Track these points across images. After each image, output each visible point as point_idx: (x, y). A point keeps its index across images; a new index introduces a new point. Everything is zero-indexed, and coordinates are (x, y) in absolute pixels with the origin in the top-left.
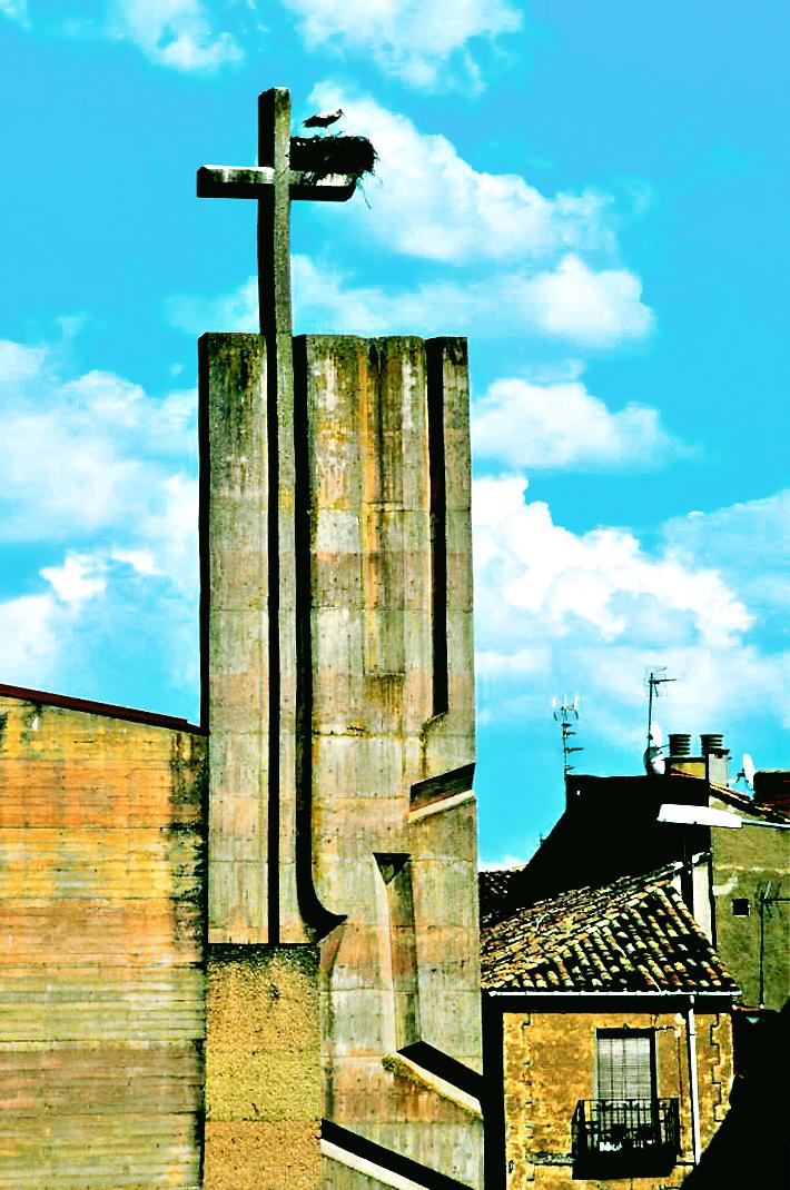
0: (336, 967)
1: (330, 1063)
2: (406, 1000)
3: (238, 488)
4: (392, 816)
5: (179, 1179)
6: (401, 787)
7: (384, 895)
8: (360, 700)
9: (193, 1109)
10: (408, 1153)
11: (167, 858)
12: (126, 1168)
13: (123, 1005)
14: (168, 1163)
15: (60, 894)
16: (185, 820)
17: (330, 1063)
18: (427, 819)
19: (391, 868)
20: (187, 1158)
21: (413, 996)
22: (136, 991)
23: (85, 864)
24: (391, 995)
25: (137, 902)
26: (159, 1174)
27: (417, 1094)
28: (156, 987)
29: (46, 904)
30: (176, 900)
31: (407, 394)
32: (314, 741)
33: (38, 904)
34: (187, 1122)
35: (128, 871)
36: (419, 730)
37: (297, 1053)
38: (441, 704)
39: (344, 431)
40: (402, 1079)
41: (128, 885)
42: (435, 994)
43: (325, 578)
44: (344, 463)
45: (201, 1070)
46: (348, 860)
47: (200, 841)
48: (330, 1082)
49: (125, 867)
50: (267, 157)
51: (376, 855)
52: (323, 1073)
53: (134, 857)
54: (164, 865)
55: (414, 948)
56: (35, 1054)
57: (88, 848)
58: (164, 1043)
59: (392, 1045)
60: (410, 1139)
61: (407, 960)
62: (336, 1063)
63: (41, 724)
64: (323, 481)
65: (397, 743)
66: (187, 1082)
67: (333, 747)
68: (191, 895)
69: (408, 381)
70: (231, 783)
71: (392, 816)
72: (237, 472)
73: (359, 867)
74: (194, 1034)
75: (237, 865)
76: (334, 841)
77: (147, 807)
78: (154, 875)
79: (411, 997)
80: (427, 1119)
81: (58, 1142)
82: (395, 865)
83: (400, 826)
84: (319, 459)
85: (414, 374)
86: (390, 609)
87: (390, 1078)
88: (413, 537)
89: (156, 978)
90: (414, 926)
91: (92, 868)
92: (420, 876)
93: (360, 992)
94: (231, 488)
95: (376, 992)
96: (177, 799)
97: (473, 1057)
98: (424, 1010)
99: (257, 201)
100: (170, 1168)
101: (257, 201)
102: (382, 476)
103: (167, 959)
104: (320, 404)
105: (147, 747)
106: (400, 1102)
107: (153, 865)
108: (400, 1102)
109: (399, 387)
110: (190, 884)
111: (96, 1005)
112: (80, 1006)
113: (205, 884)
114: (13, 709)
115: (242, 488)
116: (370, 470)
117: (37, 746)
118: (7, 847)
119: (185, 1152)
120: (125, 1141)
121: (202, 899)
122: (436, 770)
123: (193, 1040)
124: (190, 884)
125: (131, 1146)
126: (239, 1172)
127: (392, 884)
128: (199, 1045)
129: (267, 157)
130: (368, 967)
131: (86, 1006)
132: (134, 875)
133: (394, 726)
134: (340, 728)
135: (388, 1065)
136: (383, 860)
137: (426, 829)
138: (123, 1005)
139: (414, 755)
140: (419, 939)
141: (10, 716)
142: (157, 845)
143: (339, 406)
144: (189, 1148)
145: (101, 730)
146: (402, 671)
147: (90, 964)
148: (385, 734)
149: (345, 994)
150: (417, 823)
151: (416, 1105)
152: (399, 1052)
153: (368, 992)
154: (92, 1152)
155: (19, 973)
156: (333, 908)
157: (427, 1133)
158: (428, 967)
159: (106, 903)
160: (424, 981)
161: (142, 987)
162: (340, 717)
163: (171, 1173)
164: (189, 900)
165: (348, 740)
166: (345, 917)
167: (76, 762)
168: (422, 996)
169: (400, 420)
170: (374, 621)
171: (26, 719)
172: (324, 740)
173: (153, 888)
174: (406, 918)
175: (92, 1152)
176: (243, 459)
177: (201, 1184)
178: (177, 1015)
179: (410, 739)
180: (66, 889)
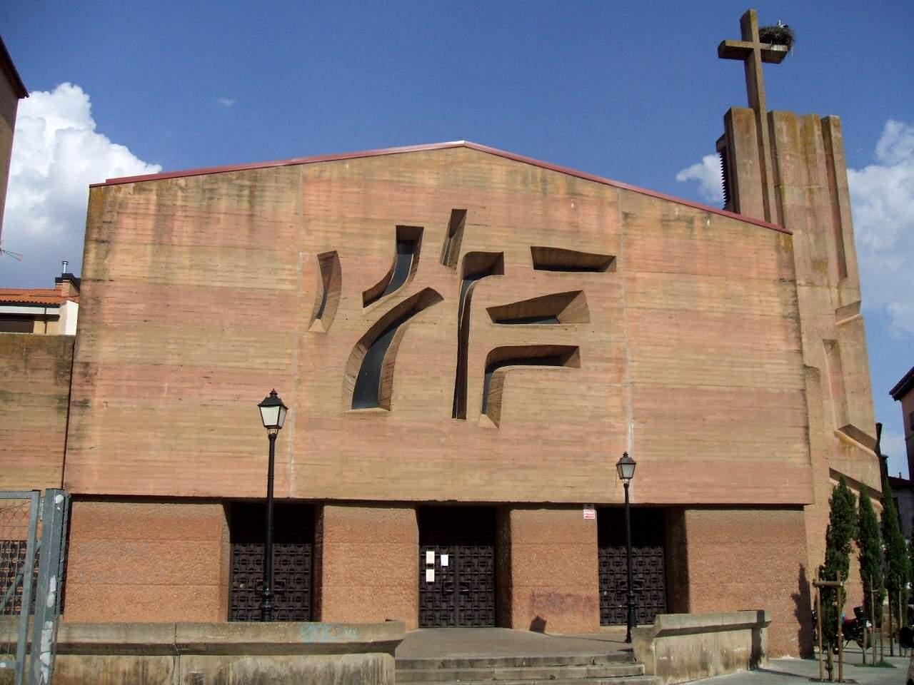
2: (840, 406)
3: (749, 174)
5: (801, 460)
6: (831, 310)
9: (802, 425)
12: (773, 453)
14: (793, 452)
15: (728, 311)
18: (843, 325)
19: (829, 347)
20: (802, 450)
21: (844, 403)
23: (739, 296)
24: (833, 404)
26: (790, 458)
27: (849, 448)
29: (722, 315)
30: (785, 317)
33: (718, 315)
34: (801, 431)
36: (836, 285)
38: (843, 272)
39: (792, 152)
40: (843, 441)
44: (793, 166)
45: (806, 405)
46: (812, 342)
47: (794, 288)
50: (746, 35)
51: (823, 340)
54: (777, 299)
56: (724, 393)
57: (740, 288)
58: (786, 391)
60: (848, 468)
63: (710, 223)
64: (785, 173)
65: (828, 291)
68: (791, 316)
71: (828, 323)
72: (748, 167)
74: (801, 386)
77: (766, 269)
78: (772, 304)
79: (843, 404)
80: (855, 458)
82: (832, 345)
83: (832, 327)
85: (819, 130)
86: (819, 234)
88: (824, 200)
90: (842, 373)
91: (743, 298)
92: (843, 350)
94: (747, 174)
96: (780, 266)
97: (872, 432)
99: (743, 61)
100: (795, 455)
101: (743, 61)
102: (809, 173)
103: (784, 348)
104: (781, 140)
105: (764, 239)
106: (843, 451)
107: (772, 299)
108: (843, 451)
109: (813, 135)
111: (750, 369)
112: (743, 369)
113: (798, 310)
114: (698, 215)
116: (804, 172)
118: (701, 285)
119: (800, 446)
121: (797, 318)
122: (845, 303)
123: (334, 671)
124: (791, 309)
128: (803, 390)
129: (746, 35)
131: (746, 369)
132: (764, 304)
133: (826, 283)
134: (802, 282)
135: (836, 435)
136: (826, 342)
137: (843, 329)
139: (835, 296)
140: (845, 378)
141: (696, 218)
142: (772, 289)
143: (788, 142)
145: (741, 228)
146: (827, 258)
147: (746, 348)
148: (822, 286)
150: (840, 326)
151: (849, 452)
152: (839, 429)
154: (757, 445)
155: (711, 350)
158: (850, 391)
159: (751, 317)
160: (849, 398)
164: (791, 317)
165: (806, 288)
169: (815, 149)
170: (812, 238)
171: (704, 220)
173: (773, 311)
175: (757, 445)
177: (811, 464)
180: (732, 308)
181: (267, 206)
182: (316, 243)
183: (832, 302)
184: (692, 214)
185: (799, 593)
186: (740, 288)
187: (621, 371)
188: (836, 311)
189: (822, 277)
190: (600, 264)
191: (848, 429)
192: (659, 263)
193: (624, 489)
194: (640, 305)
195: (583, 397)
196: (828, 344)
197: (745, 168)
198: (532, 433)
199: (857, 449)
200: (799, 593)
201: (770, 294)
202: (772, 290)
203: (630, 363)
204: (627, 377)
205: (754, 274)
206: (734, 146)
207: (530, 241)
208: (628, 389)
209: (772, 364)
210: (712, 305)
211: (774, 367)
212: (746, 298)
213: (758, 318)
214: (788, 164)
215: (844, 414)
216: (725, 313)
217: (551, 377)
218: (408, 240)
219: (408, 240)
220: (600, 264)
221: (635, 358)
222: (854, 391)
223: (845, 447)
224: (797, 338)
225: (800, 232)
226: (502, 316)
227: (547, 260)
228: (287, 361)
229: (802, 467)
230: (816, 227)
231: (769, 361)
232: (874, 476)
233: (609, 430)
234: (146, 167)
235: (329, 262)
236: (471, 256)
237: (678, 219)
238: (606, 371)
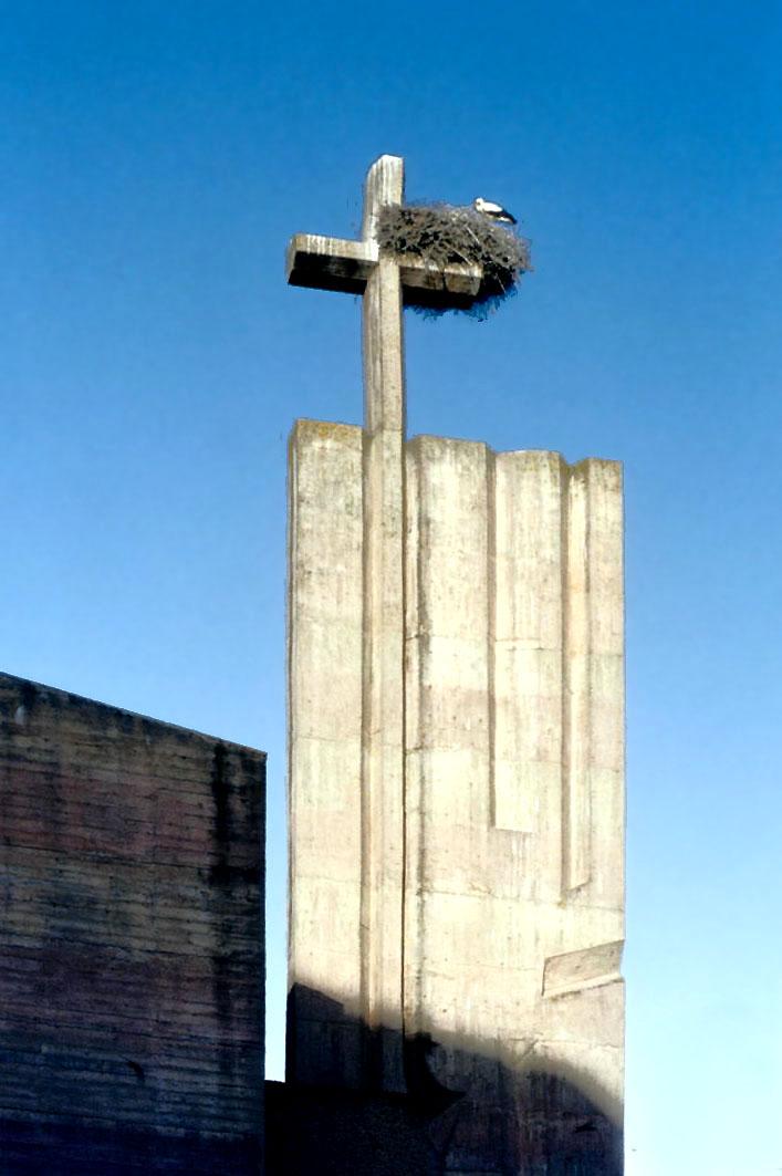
15: (57, 934)
33: (26, 943)
54: (204, 916)
107: (188, 914)
131: (96, 1076)
142: (193, 889)
181: (608, 913)
185: (573, 478)
186: (96, 882)
200: (573, 478)
201: (182, 901)
202: (191, 893)
205: (140, 848)
206: (369, 824)
209: (170, 1068)
210: (11, 916)
211: (175, 1076)
212: (110, 907)
213: (139, 957)
216: (44, 938)
224: (427, 880)
231: (165, 1061)
232: (395, 572)
234: (428, 891)
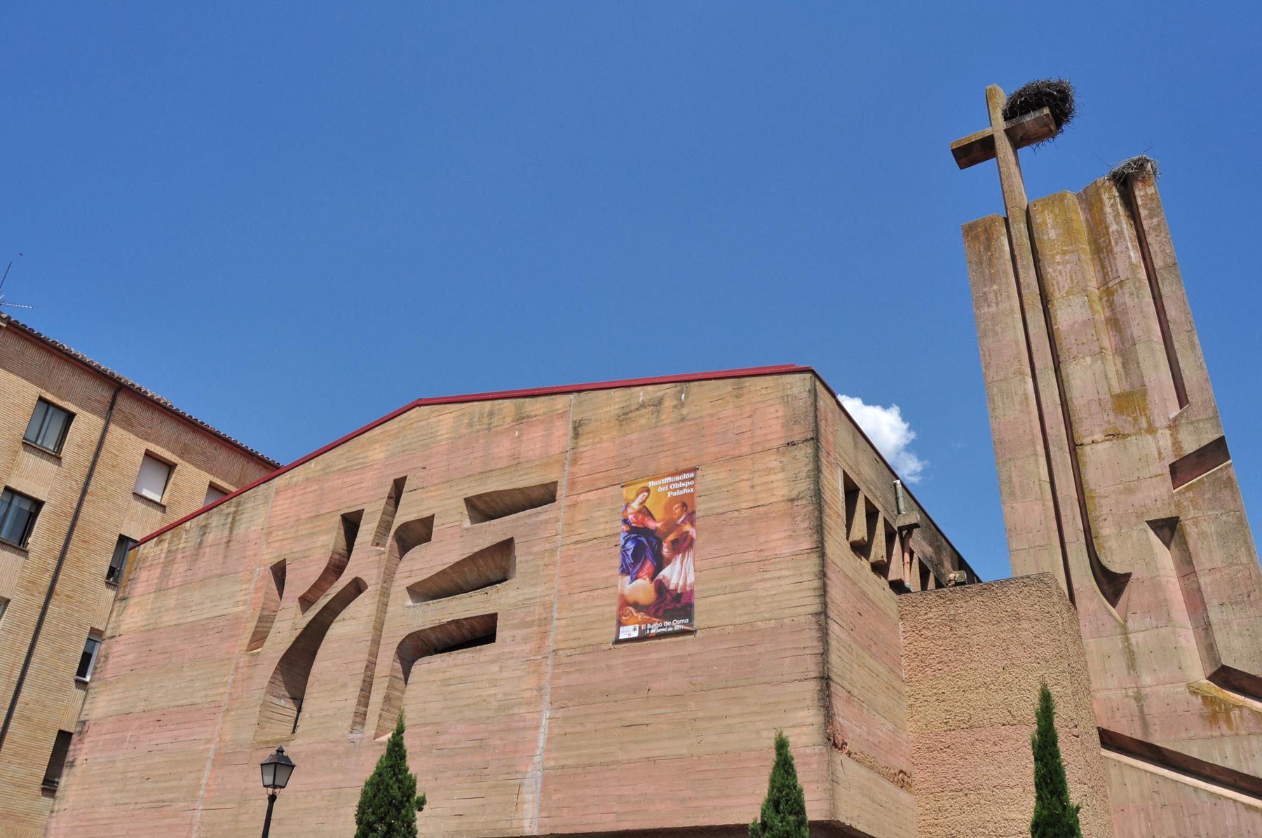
0: (1129, 614)
1: (1138, 692)
2: (1203, 633)
4: (1158, 496)
7: (1165, 558)
8: (1112, 414)
10: (1231, 764)
11: (783, 470)
13: (754, 593)
16: (796, 439)
17: (1138, 692)
20: (810, 720)
21: (1207, 627)
22: (764, 580)
25: (761, 509)
28: (778, 574)
31: (1108, 210)
32: (1079, 451)
34: (812, 687)
35: (753, 487)
37: (1043, 663)
40: (1208, 700)
41: (753, 497)
42: (1227, 624)
43: (1067, 343)
48: (1141, 711)
49: (749, 484)
52: (1133, 701)
53: (757, 475)
54: (781, 476)
55: (1199, 589)
59: (1198, 673)
60: (1229, 750)
61: (1196, 601)
62: (1143, 692)
65: (1150, 438)
66: (808, 651)
67: (1097, 454)
69: (1107, 203)
70: (1018, 493)
71: (1158, 496)
72: (991, 296)
73: (1135, 534)
75: (1032, 551)
76: (1110, 519)
78: (774, 485)
81: (701, 714)
82: (1168, 528)
84: (1050, 270)
87: (1198, 701)
89: (778, 567)
92: (1191, 531)
93: (1155, 632)
94: (989, 306)
95: (1169, 629)
98: (1220, 638)
102: (1103, 267)
105: (764, 392)
106: (1213, 718)
107: (772, 477)
108: (1213, 718)
110: (804, 486)
115: (997, 304)
117: (685, 411)
120: (755, 709)
122: (1190, 446)
125: (758, 713)
126: (1003, 770)
127: (1172, 545)
130: (1160, 609)
131: (722, 597)
132: (759, 488)
134: (1098, 436)
138: (754, 593)
140: (1202, 581)
144: (813, 711)
148: (1138, 433)
149: (1142, 634)
153: (1163, 630)
156: (1117, 569)
157: (1245, 743)
158: (1215, 602)
160: (1215, 615)
161: (767, 576)
162: (1097, 429)
163: (798, 735)
165: (1107, 444)
166: (1129, 575)
167: (712, 416)
168: (1214, 627)
172: (1087, 449)
174: (1187, 565)
176: (995, 287)
178: (798, 595)
179: (1160, 431)
182: (271, 558)
183: (1160, 454)
184: (660, 394)
187: (544, 635)
188: (1173, 468)
189: (1135, 419)
190: (545, 496)
191: (1225, 677)
192: (609, 473)
193: (267, 802)
194: (578, 538)
195: (494, 683)
196: (1162, 527)
197: (986, 300)
198: (427, 742)
199: (1246, 712)
203: (556, 622)
204: (550, 644)
207: (463, 492)
208: (549, 661)
214: (1059, 268)
215: (1210, 648)
217: (460, 662)
218: (351, 524)
219: (351, 524)
220: (545, 496)
221: (564, 614)
222: (1226, 601)
223: (1215, 713)
225: (1089, 359)
226: (425, 592)
227: (484, 508)
228: (221, 690)
229: (809, 751)
230: (1123, 343)
233: (517, 725)
235: (280, 572)
236: (405, 527)
237: (643, 406)
238: (526, 640)
